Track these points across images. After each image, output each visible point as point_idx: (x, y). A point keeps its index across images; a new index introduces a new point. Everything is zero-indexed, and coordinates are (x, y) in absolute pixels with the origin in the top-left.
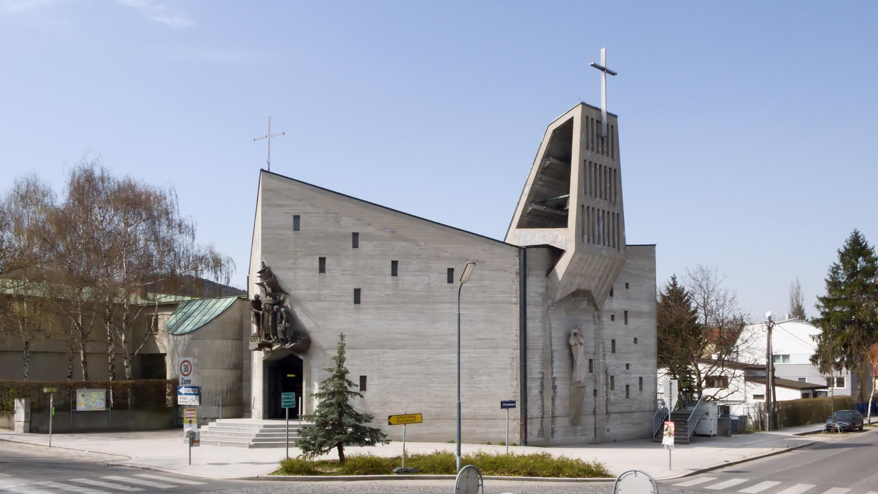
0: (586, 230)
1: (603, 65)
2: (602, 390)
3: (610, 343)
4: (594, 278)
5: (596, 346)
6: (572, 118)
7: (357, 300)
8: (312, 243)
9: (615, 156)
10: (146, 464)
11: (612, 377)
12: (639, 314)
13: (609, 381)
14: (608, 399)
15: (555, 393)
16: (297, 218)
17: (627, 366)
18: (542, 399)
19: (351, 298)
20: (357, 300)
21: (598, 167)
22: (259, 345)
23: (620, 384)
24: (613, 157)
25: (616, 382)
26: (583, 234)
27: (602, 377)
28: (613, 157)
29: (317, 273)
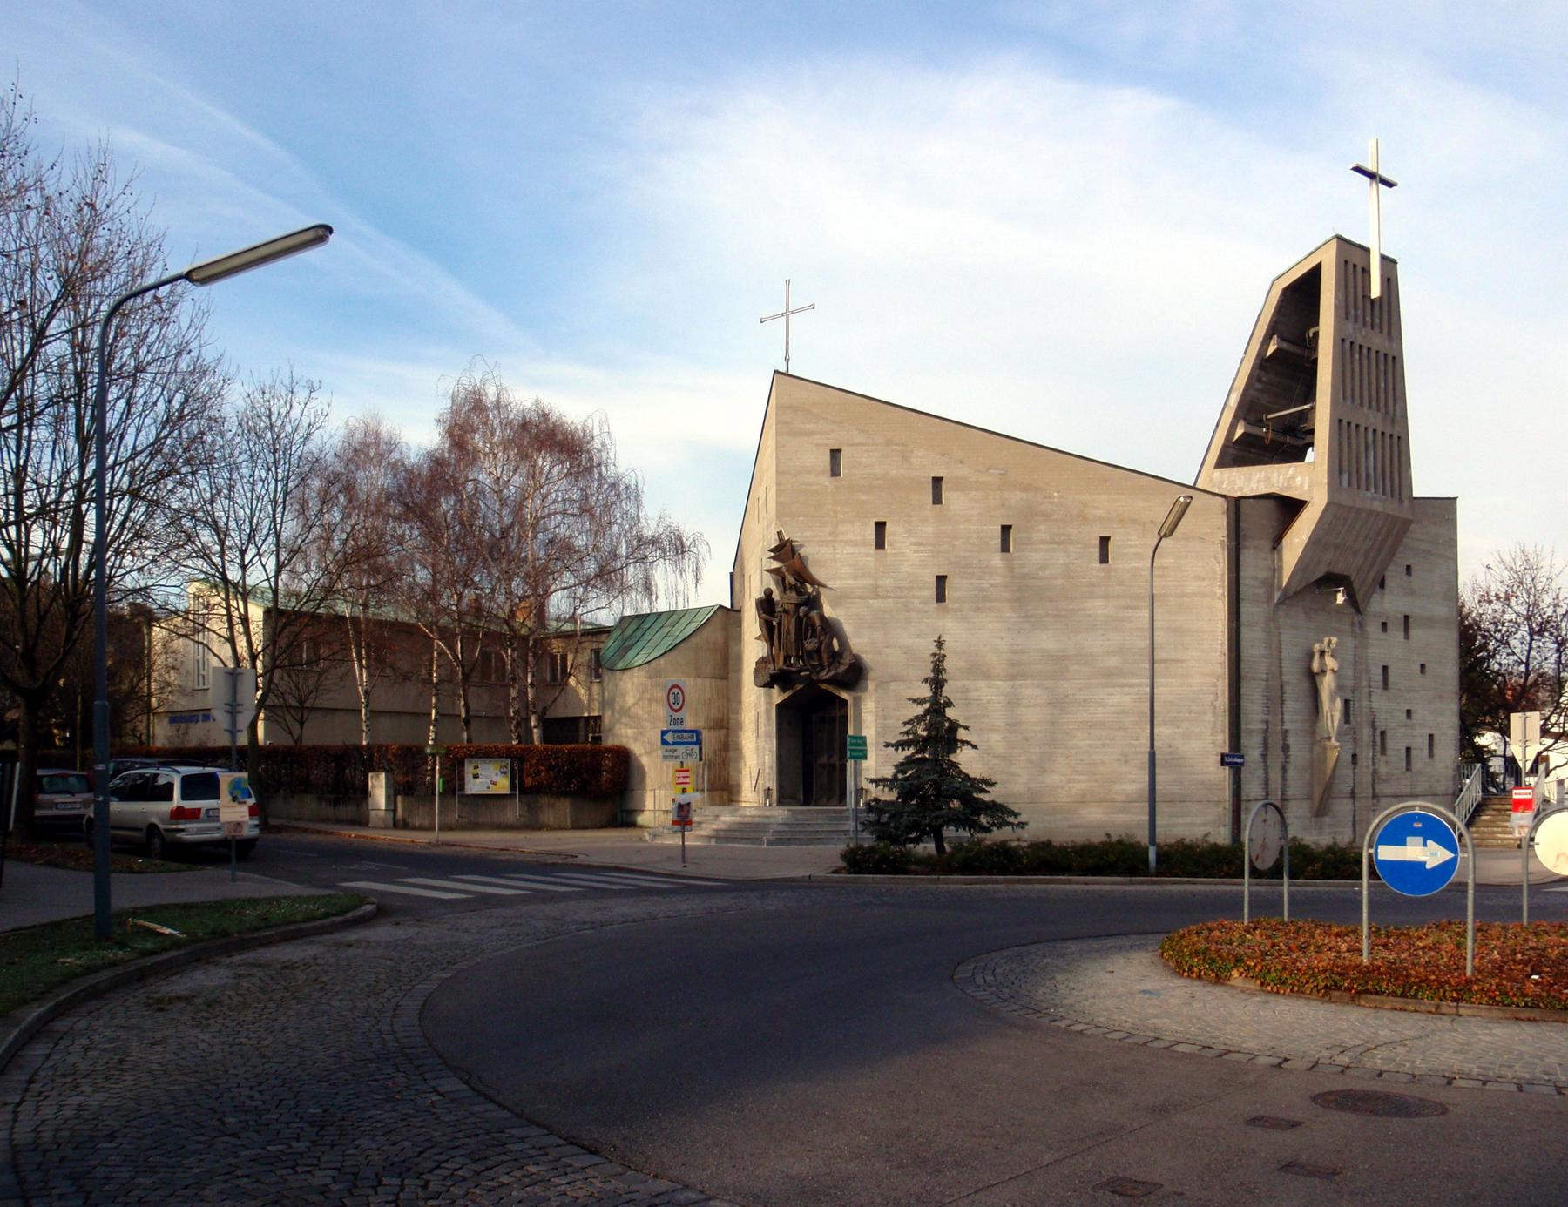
0: (1345, 464)
1: (1371, 167)
2: (1366, 755)
3: (1380, 671)
4: (1355, 553)
5: (1357, 678)
6: (1319, 266)
7: (940, 597)
8: (864, 498)
9: (1394, 333)
10: (618, 861)
11: (1383, 733)
12: (1430, 622)
13: (1378, 739)
14: (1375, 772)
15: (1287, 757)
16: (835, 454)
17: (1409, 712)
18: (1266, 767)
19: (931, 592)
20: (940, 597)
21: (1365, 351)
22: (772, 676)
23: (1396, 746)
24: (1389, 334)
25: (1390, 743)
26: (1341, 473)
27: (1366, 732)
28: (1389, 334)
29: (872, 549)
